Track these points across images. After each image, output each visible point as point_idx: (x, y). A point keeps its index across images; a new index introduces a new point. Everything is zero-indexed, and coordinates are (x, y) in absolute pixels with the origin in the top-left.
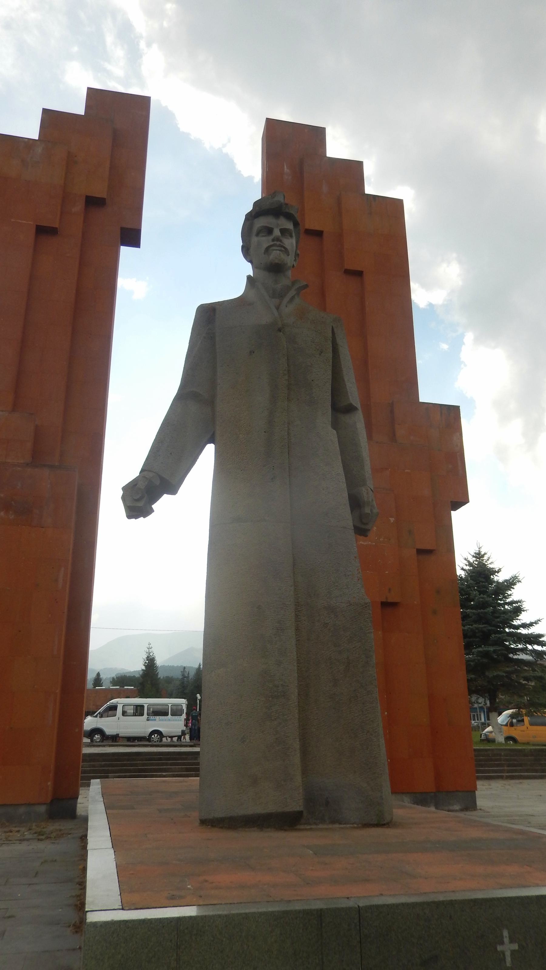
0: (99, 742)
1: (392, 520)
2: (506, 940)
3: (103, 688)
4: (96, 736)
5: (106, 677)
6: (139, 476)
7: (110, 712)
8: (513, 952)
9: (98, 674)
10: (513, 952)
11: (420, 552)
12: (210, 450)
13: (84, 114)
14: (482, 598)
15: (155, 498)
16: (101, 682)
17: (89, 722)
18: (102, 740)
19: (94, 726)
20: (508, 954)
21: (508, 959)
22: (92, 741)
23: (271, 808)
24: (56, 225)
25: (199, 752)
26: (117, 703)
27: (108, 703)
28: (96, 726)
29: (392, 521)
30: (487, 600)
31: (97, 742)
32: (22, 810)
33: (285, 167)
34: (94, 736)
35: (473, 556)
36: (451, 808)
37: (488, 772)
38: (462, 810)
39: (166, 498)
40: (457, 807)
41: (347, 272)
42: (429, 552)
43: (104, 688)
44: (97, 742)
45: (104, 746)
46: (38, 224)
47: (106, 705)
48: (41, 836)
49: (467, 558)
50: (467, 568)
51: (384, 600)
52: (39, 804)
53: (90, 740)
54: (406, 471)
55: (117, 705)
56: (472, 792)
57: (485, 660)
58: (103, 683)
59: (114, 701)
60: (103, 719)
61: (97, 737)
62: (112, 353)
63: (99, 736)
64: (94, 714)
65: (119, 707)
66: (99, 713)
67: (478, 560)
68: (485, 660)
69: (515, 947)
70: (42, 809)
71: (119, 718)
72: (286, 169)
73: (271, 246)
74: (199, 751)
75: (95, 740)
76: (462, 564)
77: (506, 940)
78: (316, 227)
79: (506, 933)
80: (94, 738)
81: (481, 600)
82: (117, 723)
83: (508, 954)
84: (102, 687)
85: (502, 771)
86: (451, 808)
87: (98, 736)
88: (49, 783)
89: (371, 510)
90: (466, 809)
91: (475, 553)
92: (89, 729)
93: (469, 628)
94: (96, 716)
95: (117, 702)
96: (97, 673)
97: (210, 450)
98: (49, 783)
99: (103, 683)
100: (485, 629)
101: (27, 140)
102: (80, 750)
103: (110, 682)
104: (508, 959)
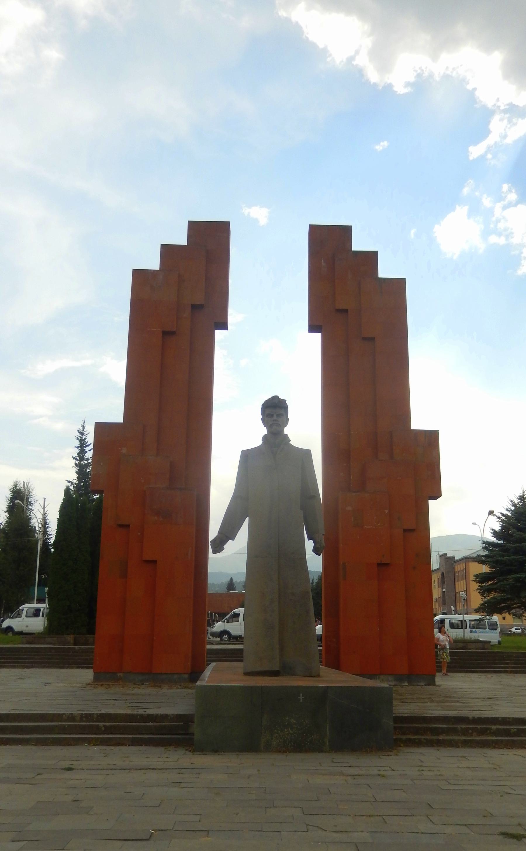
0: (227, 641)
1: (386, 511)
2: (301, 696)
3: (236, 592)
4: (225, 636)
5: (239, 581)
6: (218, 535)
7: (234, 619)
8: (303, 699)
9: (231, 580)
10: (303, 699)
11: (405, 530)
12: (247, 519)
13: (185, 243)
14: (519, 535)
15: (225, 542)
16: (234, 586)
17: (219, 626)
18: (229, 640)
19: (222, 629)
20: (301, 699)
21: (301, 701)
22: (222, 640)
23: (267, 669)
24: (174, 330)
25: (242, 649)
26: (239, 611)
27: (232, 612)
28: (224, 629)
29: (386, 512)
30: (523, 536)
31: (225, 641)
32: (176, 676)
33: (323, 262)
34: (223, 636)
35: (519, 499)
36: (419, 684)
37: (499, 668)
38: (425, 685)
39: (230, 541)
40: (422, 684)
41: (365, 339)
42: (412, 530)
43: (237, 592)
44: (225, 641)
45: (228, 644)
46: (164, 330)
47: (231, 613)
48: (185, 687)
49: (513, 500)
50: (513, 508)
51: (380, 562)
52: (184, 674)
53: (220, 639)
54: (398, 478)
55: (239, 613)
56: (434, 676)
57: (519, 584)
58: (235, 587)
59: (237, 610)
60: (230, 624)
61: (225, 637)
62: (230, 273)
63: (227, 637)
64: (222, 620)
65: (241, 615)
66: (226, 619)
67: (522, 501)
68: (519, 584)
69: (303, 698)
70: (186, 676)
71: (241, 623)
72: (323, 264)
73: (272, 424)
74: (322, 649)
75: (224, 639)
76: (509, 504)
77: (301, 696)
78: (344, 307)
79: (301, 694)
80: (223, 638)
81: (518, 536)
82: (240, 627)
83: (301, 699)
84: (235, 591)
85: (507, 668)
86: (419, 684)
87: (226, 636)
88: (189, 663)
89: (320, 545)
90: (428, 685)
91: (520, 496)
92: (219, 631)
93: (507, 559)
94: (224, 622)
95: (239, 611)
96: (230, 578)
97: (247, 519)
98: (189, 663)
99: (235, 587)
100: (520, 560)
101: (152, 271)
102: (205, 647)
103: (243, 586)
104: (301, 701)
